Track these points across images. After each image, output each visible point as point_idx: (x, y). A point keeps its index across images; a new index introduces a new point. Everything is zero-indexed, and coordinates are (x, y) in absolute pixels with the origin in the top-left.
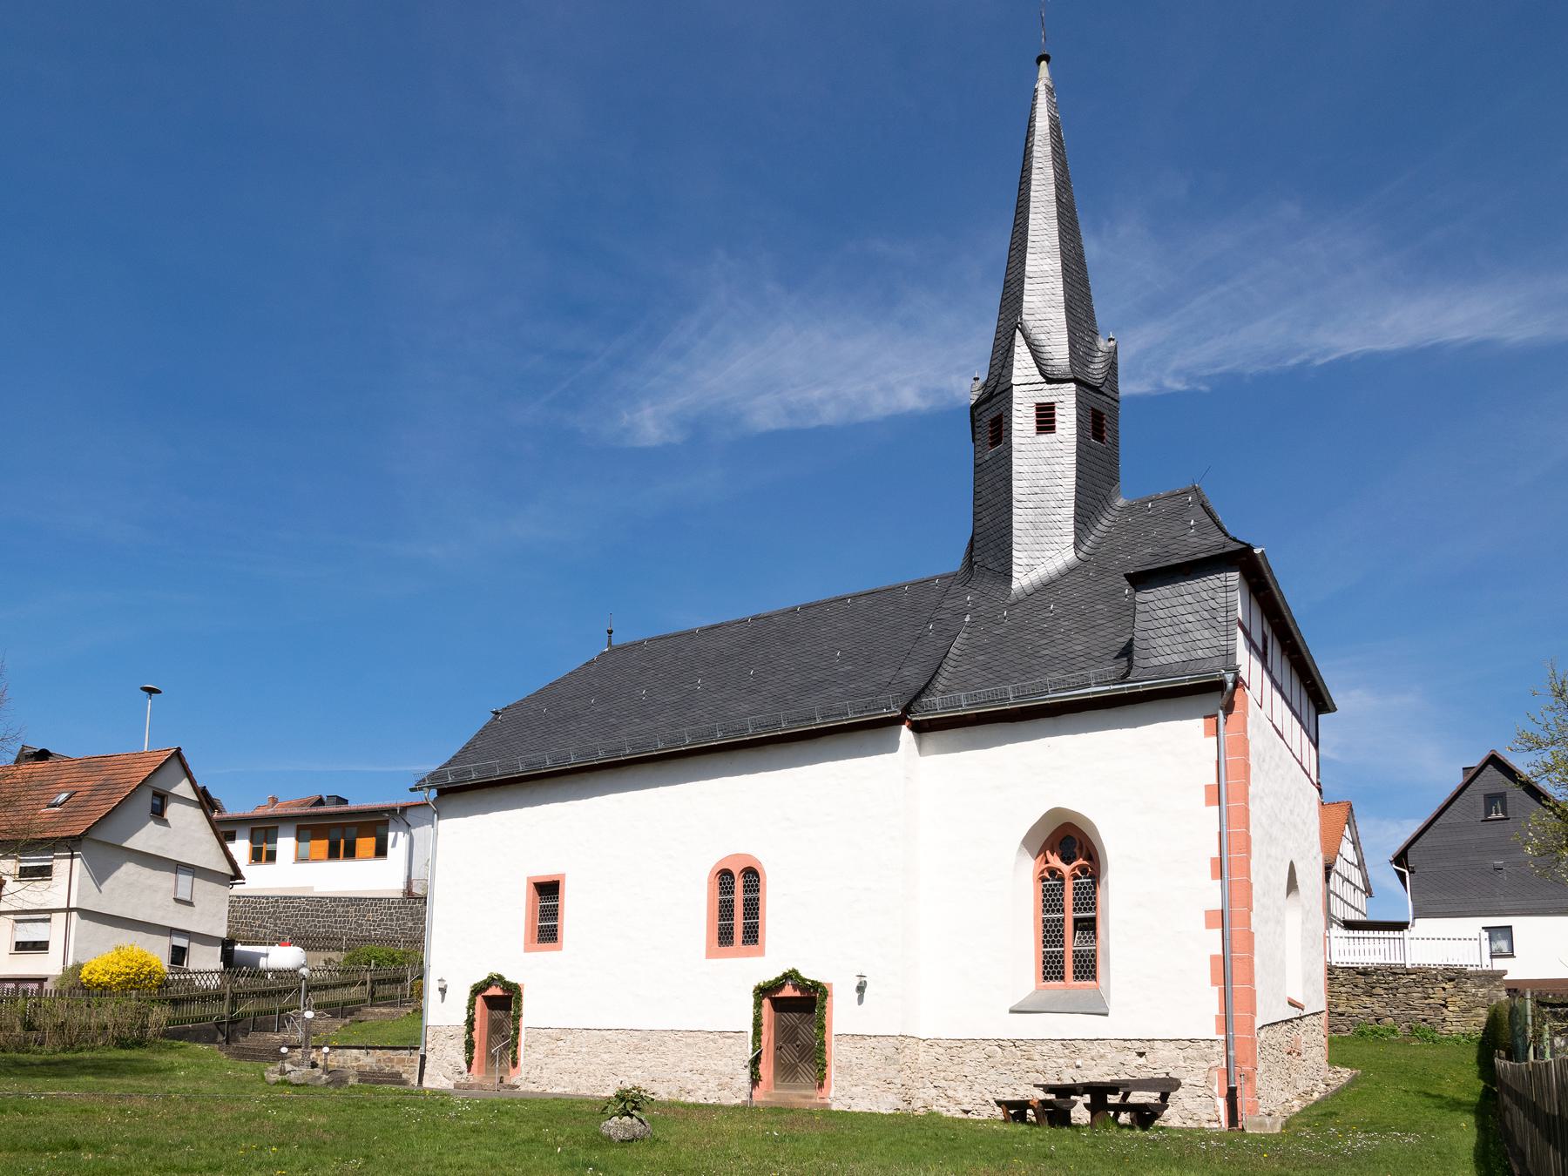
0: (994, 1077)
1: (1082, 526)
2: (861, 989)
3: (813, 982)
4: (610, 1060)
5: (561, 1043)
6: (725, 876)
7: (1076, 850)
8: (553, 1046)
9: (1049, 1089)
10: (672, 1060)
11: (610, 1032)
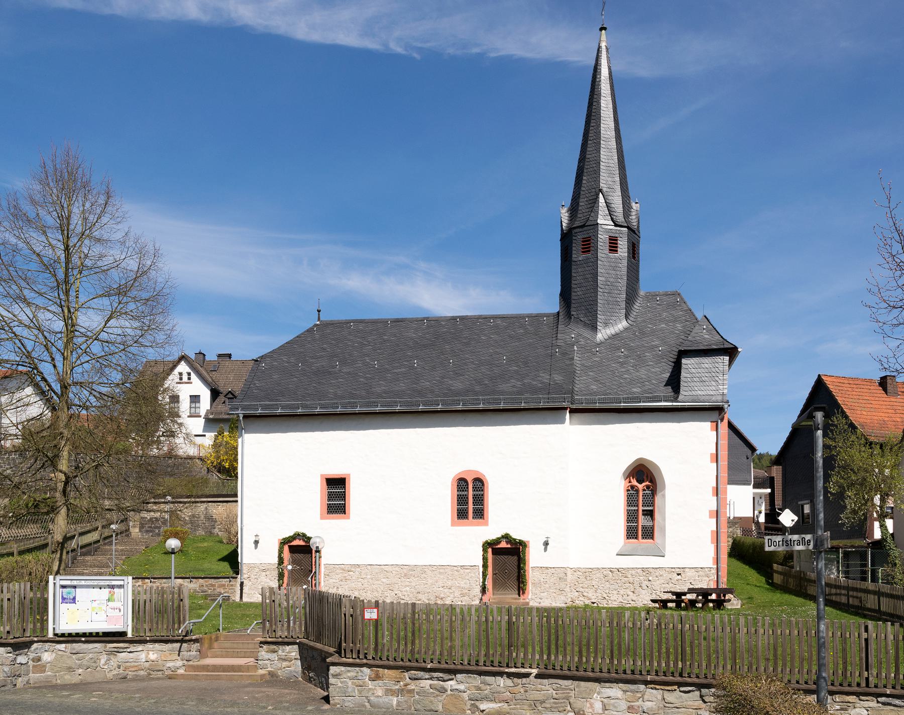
0: (608, 586)
1: (628, 305)
2: (546, 544)
3: (520, 540)
4: (388, 582)
5: (351, 573)
6: (462, 483)
7: (645, 478)
8: (345, 575)
9: (674, 593)
10: (430, 581)
11: (387, 567)
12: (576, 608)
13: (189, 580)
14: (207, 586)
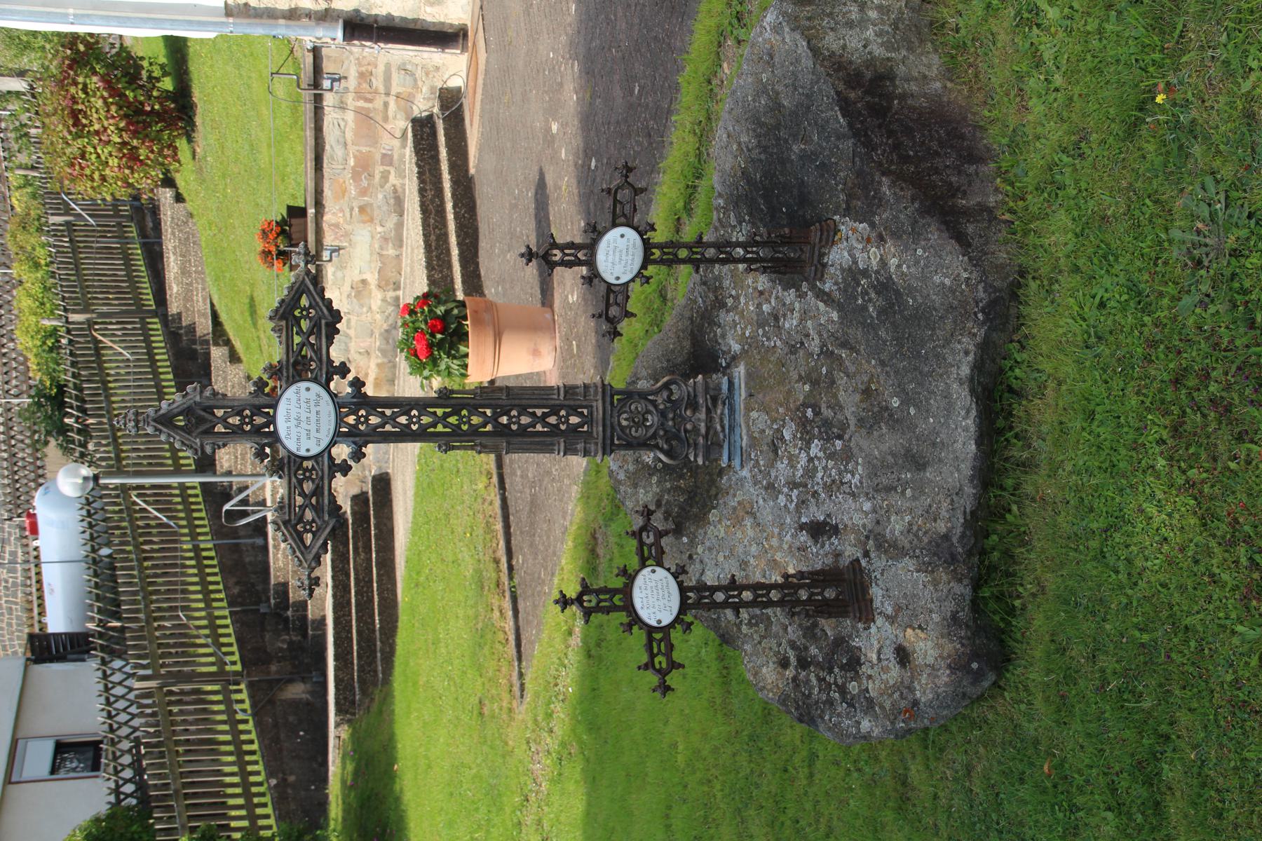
14: (363, 192)
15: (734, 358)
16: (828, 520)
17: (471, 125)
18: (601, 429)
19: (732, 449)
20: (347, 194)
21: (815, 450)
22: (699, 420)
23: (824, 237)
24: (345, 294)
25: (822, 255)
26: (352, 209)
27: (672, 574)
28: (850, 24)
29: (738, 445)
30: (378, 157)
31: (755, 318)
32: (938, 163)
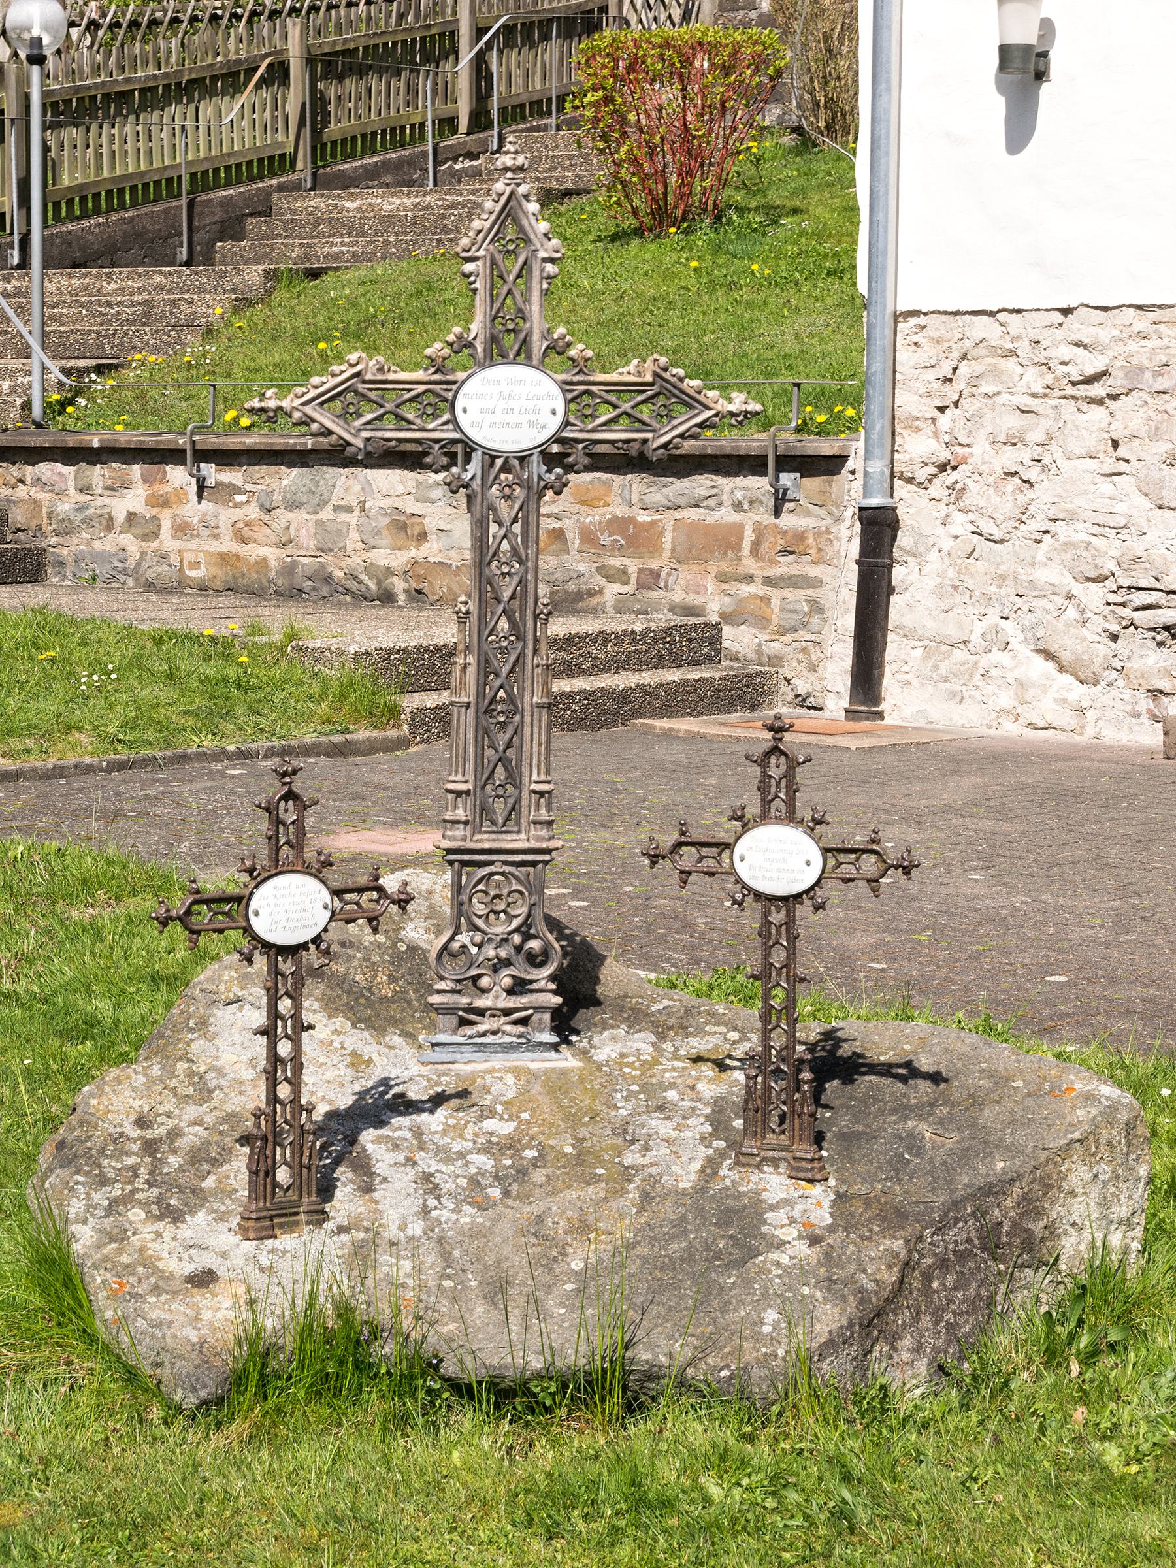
12: (890, 568)
13: (759, 484)
14: (588, 537)
15: (585, 1052)
16: (377, 1180)
17: (722, 724)
18: (487, 846)
19: (451, 1049)
20: (585, 508)
21: (483, 1162)
22: (497, 997)
23: (804, 1164)
24: (398, 503)
25: (775, 1162)
26: (558, 518)
27: (319, 936)
28: (1104, 1203)
29: (458, 1056)
30: (654, 564)
31: (654, 1081)
32: (926, 1321)
